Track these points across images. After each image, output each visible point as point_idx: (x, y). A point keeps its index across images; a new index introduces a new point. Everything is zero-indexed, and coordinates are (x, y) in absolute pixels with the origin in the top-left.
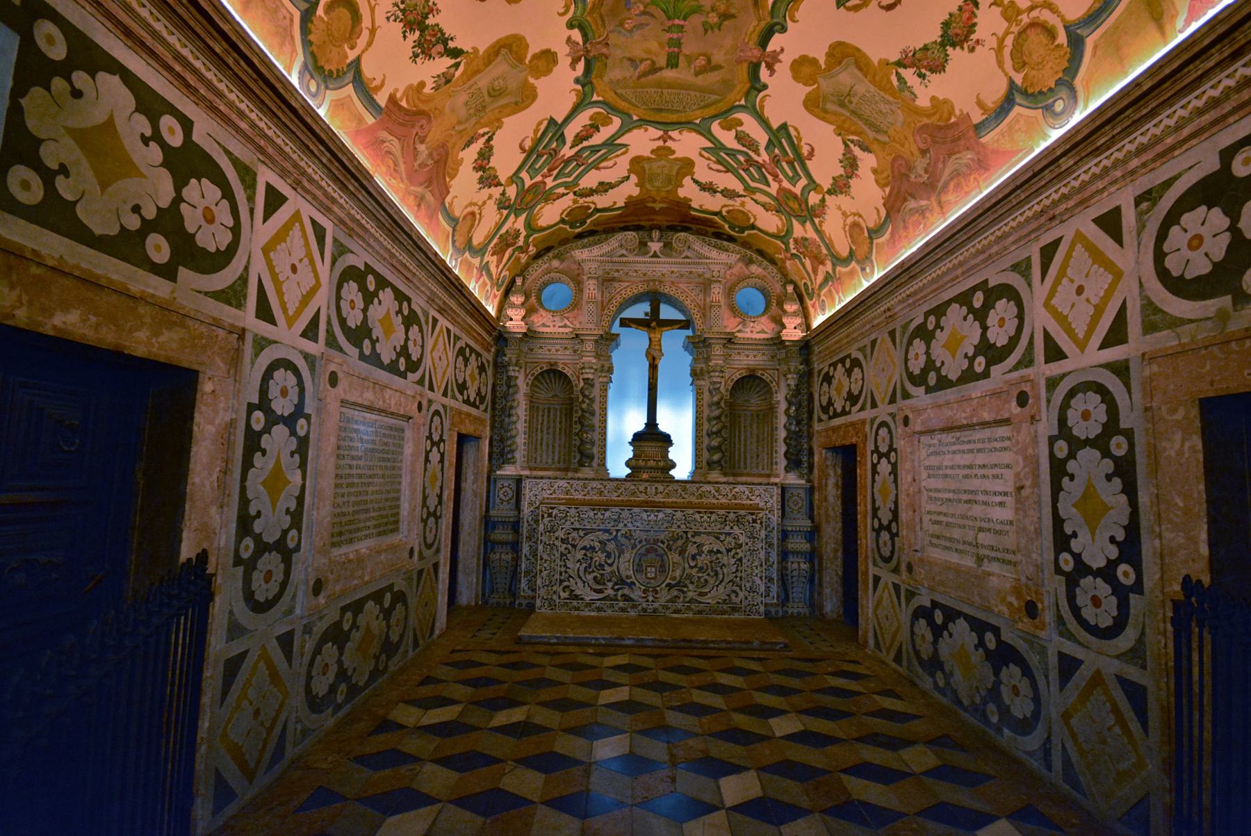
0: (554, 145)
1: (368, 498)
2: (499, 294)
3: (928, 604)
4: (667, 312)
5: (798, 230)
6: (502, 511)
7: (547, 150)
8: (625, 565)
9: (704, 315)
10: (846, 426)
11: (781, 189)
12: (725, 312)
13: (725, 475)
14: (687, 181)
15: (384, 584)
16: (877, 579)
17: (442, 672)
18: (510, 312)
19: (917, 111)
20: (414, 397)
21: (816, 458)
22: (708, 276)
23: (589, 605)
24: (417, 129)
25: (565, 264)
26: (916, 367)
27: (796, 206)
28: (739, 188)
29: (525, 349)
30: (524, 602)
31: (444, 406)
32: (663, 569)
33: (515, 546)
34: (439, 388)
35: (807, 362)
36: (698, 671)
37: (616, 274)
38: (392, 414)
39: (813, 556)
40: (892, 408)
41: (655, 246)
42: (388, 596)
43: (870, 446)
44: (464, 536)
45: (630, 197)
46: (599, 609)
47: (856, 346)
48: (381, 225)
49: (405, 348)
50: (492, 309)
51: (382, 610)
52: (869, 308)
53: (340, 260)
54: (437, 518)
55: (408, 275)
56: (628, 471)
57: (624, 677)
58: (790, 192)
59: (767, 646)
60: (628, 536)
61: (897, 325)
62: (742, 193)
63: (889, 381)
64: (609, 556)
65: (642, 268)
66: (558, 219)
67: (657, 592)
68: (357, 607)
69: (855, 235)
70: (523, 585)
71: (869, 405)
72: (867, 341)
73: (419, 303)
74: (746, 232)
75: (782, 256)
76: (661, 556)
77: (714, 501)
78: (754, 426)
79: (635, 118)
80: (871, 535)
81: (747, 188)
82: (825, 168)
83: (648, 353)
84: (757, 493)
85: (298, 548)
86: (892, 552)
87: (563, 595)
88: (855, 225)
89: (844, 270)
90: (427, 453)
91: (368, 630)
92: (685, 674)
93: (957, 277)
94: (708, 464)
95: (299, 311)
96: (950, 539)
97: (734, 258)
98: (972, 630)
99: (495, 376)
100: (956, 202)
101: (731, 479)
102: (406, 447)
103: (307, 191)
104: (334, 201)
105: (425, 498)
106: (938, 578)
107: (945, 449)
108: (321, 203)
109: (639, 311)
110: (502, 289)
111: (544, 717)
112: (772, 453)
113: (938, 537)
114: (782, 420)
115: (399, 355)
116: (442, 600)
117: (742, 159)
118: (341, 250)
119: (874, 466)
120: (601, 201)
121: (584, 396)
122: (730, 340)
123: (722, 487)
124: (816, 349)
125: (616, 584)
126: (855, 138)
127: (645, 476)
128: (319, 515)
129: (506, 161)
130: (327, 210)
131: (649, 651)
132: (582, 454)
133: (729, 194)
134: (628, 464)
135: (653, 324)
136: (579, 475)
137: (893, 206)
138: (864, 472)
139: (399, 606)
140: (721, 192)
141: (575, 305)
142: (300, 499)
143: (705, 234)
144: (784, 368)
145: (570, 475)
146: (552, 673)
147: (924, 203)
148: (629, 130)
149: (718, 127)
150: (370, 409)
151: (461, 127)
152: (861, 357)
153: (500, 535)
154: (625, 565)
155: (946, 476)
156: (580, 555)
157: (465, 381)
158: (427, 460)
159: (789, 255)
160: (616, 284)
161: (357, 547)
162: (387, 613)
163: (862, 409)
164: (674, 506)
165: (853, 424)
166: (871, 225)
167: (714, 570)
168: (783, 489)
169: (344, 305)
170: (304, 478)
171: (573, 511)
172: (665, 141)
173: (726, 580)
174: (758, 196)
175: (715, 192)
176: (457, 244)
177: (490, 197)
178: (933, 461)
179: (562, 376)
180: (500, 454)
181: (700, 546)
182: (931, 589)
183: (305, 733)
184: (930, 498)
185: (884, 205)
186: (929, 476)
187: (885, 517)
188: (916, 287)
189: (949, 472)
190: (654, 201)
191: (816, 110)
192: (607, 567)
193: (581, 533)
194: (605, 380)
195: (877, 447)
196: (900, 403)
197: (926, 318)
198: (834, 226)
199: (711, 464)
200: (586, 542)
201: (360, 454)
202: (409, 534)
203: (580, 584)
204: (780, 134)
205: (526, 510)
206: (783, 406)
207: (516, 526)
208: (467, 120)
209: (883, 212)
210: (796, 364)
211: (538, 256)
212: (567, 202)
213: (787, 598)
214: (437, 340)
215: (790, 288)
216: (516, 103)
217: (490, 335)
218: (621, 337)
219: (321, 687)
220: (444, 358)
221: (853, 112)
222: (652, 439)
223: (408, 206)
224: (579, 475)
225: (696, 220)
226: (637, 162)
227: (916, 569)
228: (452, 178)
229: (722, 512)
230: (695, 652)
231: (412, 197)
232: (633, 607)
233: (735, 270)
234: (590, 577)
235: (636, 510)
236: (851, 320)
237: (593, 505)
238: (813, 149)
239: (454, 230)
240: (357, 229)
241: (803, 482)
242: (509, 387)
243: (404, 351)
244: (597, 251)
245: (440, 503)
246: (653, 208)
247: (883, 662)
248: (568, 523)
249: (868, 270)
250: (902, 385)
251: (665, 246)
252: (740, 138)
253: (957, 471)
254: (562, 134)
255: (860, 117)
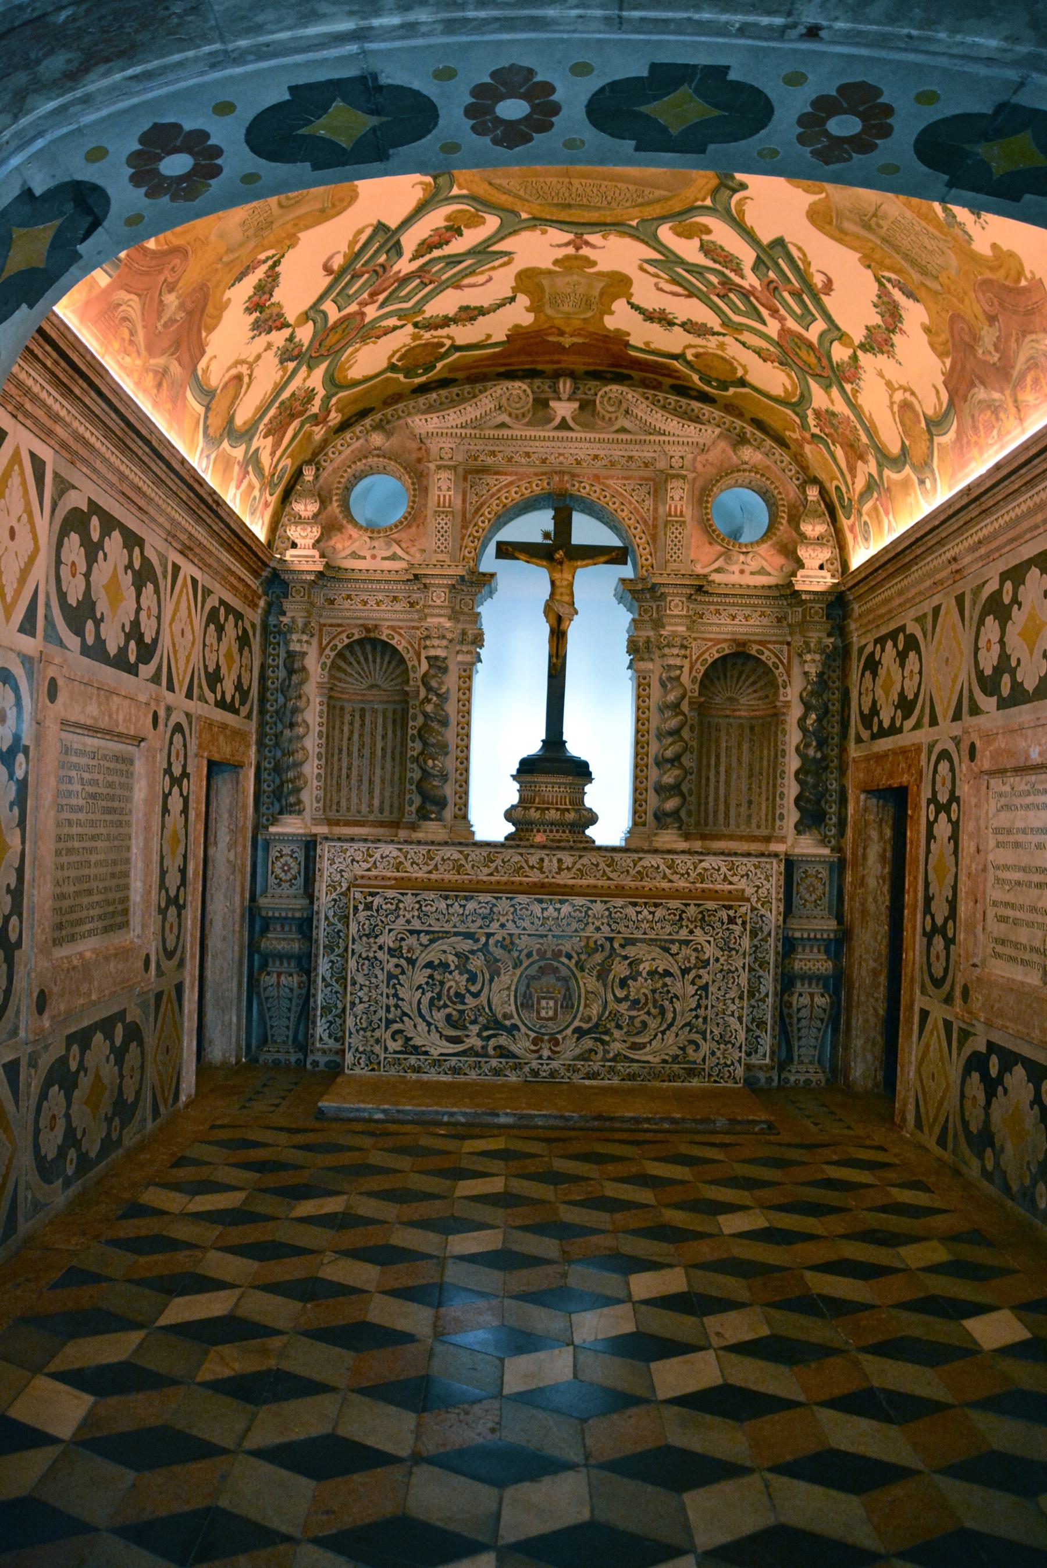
0: (382, 259)
1: (92, 871)
2: (273, 500)
3: (983, 1049)
4: (586, 530)
5: (819, 398)
6: (284, 899)
7: (370, 267)
8: (501, 994)
9: (654, 538)
10: (894, 752)
11: (784, 331)
12: (692, 533)
13: (687, 837)
14: (620, 305)
15: (115, 1009)
16: (924, 1014)
17: (199, 1151)
18: (294, 533)
19: (975, 258)
20: (148, 704)
21: (851, 810)
22: (662, 465)
23: (436, 1063)
24: (166, 273)
25: (394, 440)
26: (988, 662)
27: (813, 360)
28: (714, 322)
29: (319, 600)
30: (323, 1059)
31: (188, 715)
32: (568, 1003)
33: (305, 964)
34: (181, 684)
35: (840, 630)
36: (615, 1159)
37: (490, 460)
38: (120, 735)
39: (837, 984)
40: (956, 729)
41: (563, 409)
42: (119, 1030)
43: (926, 793)
44: (214, 943)
45: (517, 327)
46: (455, 1071)
47: (912, 613)
48: (108, 431)
49: (136, 623)
50: (259, 530)
51: (113, 1048)
52: (931, 549)
53: (61, 503)
54: (181, 908)
55: (142, 503)
56: (511, 828)
57: (497, 1166)
58: (800, 336)
59: (738, 1128)
60: (507, 945)
61: (966, 586)
62: (717, 328)
63: (954, 681)
64: (472, 979)
65: (540, 449)
66: (384, 364)
67: (557, 1043)
68: (82, 1039)
69: (908, 422)
70: (319, 1031)
71: (926, 719)
72: (927, 607)
73: (155, 545)
74: (732, 391)
75: (796, 435)
76: (566, 980)
77: (665, 885)
78: (745, 747)
79: (524, 216)
80: (919, 941)
81: (726, 323)
82: (853, 304)
83: (548, 610)
84: (742, 870)
85: (19, 944)
86: (946, 970)
87: (393, 1046)
88: (906, 406)
89: (895, 476)
90: (166, 797)
91: (98, 1077)
92: (596, 1163)
93: (1037, 527)
94: (656, 817)
95: (18, 593)
96: (1016, 945)
97: (710, 433)
98: (1029, 1081)
99: (264, 651)
100: (1036, 406)
101: (697, 845)
102: (136, 787)
103: (27, 414)
104: (56, 418)
105: (163, 873)
106: (997, 1005)
107: (1018, 801)
108: (42, 427)
109: (534, 527)
110: (279, 490)
111: (367, 1208)
112: (774, 797)
113: (1003, 943)
114: (794, 737)
115: (128, 637)
116: (189, 1045)
117: (714, 280)
118: (63, 486)
119: (930, 825)
120: (463, 334)
121: (429, 689)
122: (700, 589)
123: (679, 859)
124: (857, 609)
125: (486, 1028)
126: (893, 276)
127: (539, 838)
128: (40, 895)
129: (300, 285)
130: (46, 434)
131: (541, 1133)
132: (425, 797)
133: (689, 327)
134: (509, 815)
135: (559, 555)
136: (420, 835)
137: (959, 385)
138: (915, 834)
139: (133, 1046)
140: (683, 325)
141: (414, 518)
142: (20, 871)
143: (658, 386)
144: (798, 641)
145: (403, 834)
146: (376, 1158)
147: (997, 395)
148: (515, 232)
149: (670, 234)
150: (92, 730)
151: (231, 257)
152: (919, 635)
153: (278, 941)
154: (501, 994)
155: (1017, 845)
156: (421, 977)
157: (218, 667)
158: (165, 810)
159: (808, 436)
160: (491, 479)
161: (80, 949)
162: (119, 1055)
163: (917, 726)
164: (592, 893)
165: (904, 751)
166: (930, 412)
167: (659, 1005)
168: (790, 864)
169: (65, 571)
170: (23, 843)
171: (409, 900)
172: (578, 249)
173: (680, 1022)
174: (746, 337)
175: (671, 324)
176: (211, 431)
177: (269, 346)
178: (1003, 820)
179: (387, 648)
180: (277, 794)
181: (634, 964)
182: (989, 1024)
183: (37, 1206)
184: (998, 880)
185: (945, 383)
186: (998, 845)
187: (940, 910)
188: (990, 528)
189: (1020, 838)
190: (562, 333)
191: (828, 227)
192: (469, 999)
193: (425, 939)
194: (468, 658)
195: (934, 793)
196: (967, 720)
197: (1002, 585)
198: (874, 398)
199: (661, 818)
200: (433, 955)
201: (81, 802)
202: (142, 931)
203: (422, 1027)
204: (773, 253)
205: (324, 899)
206: (796, 711)
207: (306, 925)
208: (242, 245)
209: (945, 397)
210: (818, 635)
211: (344, 426)
212: (403, 338)
213: (790, 1059)
214: (178, 602)
215: (813, 493)
216: (322, 211)
217: (256, 574)
218: (500, 578)
219: (50, 1151)
220: (188, 630)
221: (884, 240)
222: (553, 768)
223: (145, 391)
224: (420, 835)
225: (636, 364)
226: (529, 281)
227: (973, 995)
228: (211, 329)
229: (674, 904)
230: (617, 1136)
231: (151, 374)
232: (516, 1067)
233: (713, 455)
234: (439, 1016)
235: (522, 898)
236: (907, 566)
237: (443, 889)
238: (830, 281)
239: (208, 409)
240: (83, 452)
241: (826, 851)
242: (291, 672)
243: (134, 632)
244: (454, 418)
245: (184, 882)
246: (559, 344)
247: (923, 1147)
248: (401, 921)
249: (928, 484)
250: (971, 691)
251: (582, 407)
252: (706, 249)
253: (1030, 838)
254: (398, 242)
255: (896, 248)
